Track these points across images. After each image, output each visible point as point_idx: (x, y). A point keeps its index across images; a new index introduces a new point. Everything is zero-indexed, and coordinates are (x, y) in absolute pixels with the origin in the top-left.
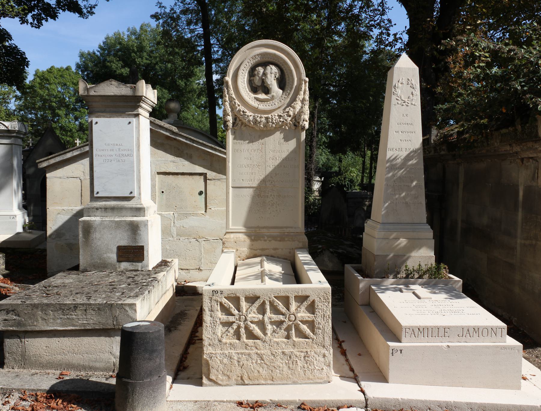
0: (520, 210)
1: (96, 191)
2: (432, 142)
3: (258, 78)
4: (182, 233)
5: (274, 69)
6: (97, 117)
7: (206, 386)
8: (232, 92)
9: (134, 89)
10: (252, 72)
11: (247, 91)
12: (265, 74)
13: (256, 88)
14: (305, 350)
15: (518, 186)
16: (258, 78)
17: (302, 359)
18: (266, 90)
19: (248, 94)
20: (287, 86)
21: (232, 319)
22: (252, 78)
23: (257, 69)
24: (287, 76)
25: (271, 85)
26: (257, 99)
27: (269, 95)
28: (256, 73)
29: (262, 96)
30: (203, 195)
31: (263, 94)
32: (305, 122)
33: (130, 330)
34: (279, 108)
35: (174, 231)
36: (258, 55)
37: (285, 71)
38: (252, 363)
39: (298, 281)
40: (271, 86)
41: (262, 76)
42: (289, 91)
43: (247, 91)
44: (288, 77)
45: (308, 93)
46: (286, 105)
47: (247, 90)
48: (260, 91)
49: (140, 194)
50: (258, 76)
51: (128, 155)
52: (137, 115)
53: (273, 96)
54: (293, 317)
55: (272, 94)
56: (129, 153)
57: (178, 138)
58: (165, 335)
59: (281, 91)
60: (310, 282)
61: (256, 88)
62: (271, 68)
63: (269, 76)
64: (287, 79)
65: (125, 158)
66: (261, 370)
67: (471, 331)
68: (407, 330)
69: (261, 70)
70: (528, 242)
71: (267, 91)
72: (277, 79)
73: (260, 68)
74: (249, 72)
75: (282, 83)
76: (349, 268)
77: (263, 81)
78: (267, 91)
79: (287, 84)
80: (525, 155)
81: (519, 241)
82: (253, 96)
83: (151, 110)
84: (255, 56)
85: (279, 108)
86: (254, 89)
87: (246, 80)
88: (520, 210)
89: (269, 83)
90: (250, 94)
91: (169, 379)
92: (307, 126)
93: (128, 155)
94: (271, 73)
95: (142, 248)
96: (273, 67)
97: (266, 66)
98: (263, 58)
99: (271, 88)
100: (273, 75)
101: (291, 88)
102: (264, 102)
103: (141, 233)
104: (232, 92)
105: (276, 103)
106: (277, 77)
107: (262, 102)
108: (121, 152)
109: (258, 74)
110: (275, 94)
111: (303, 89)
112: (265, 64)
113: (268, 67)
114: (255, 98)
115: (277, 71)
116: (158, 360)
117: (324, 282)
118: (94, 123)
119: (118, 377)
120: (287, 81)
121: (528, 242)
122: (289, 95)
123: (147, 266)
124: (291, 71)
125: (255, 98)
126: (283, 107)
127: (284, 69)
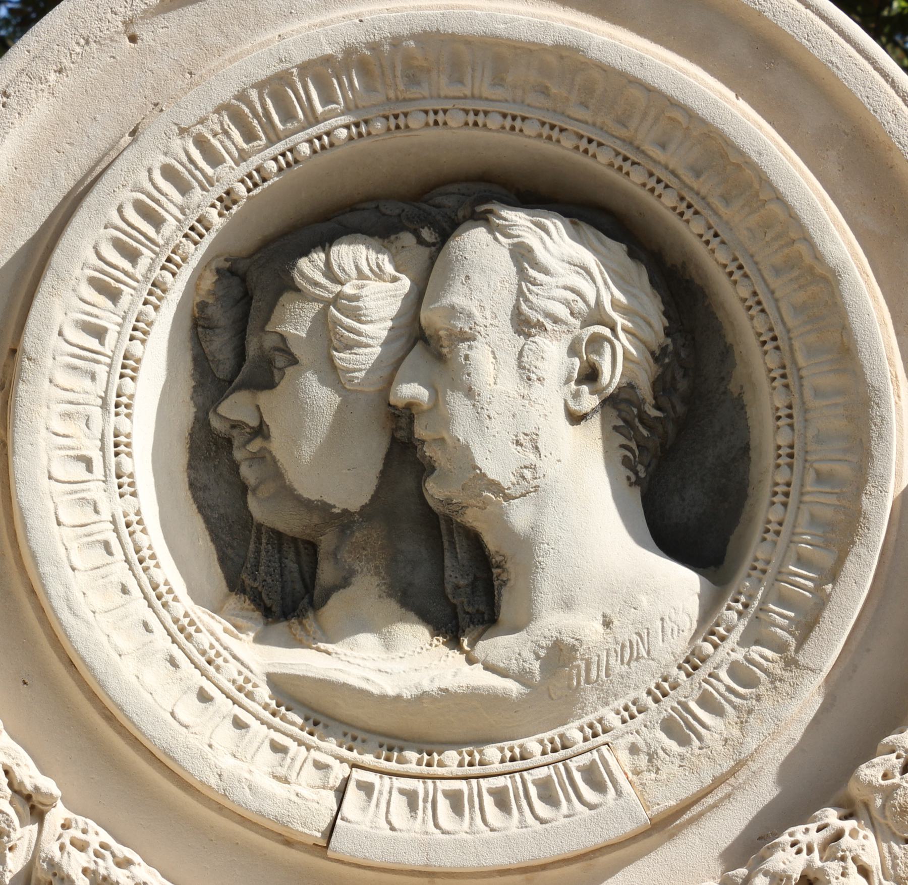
3: (321, 398)
5: (568, 261)
8: (295, 730)
10: (238, 325)
11: (157, 596)
12: (423, 340)
13: (308, 550)
16: (321, 398)
18: (455, 575)
19: (184, 630)
20: (765, 510)
22: (236, 407)
23: (310, 267)
24: (756, 363)
25: (531, 487)
26: (316, 709)
27: (498, 646)
28: (296, 323)
29: (392, 659)
31: (414, 637)
34: (664, 826)
36: (320, 70)
37: (731, 295)
40: (520, 515)
41: (391, 369)
42: (802, 581)
43: (157, 596)
44: (785, 375)
46: (762, 791)
47: (168, 571)
48: (366, 588)
50: (333, 375)
53: (559, 654)
55: (551, 622)
57: (751, 667)
58: (515, 629)
59: (682, 583)
61: (308, 550)
62: (522, 255)
63: (489, 360)
64: (765, 403)
69: (367, 283)
71: (462, 579)
72: (617, 404)
73: (351, 255)
74: (197, 325)
77: (405, 447)
78: (462, 579)
79: (768, 473)
82: (260, 657)
84: (277, 86)
85: (664, 826)
86: (275, 573)
87: (142, 427)
89: (495, 460)
90: (213, 627)
94: (523, 325)
96: (557, 244)
97: (447, 230)
98: (397, 121)
99: (526, 545)
100: (553, 356)
101: (843, 532)
102: (429, 745)
104: (295, 730)
105: (619, 762)
106: (611, 376)
107: (391, 742)
109: (329, 337)
110: (585, 627)
112: (423, 210)
113: (475, 243)
114: (288, 693)
115: (610, 295)
120: (768, 436)
122: (807, 625)
124: (824, 281)
125: (288, 693)
126: (730, 822)
127: (712, 262)
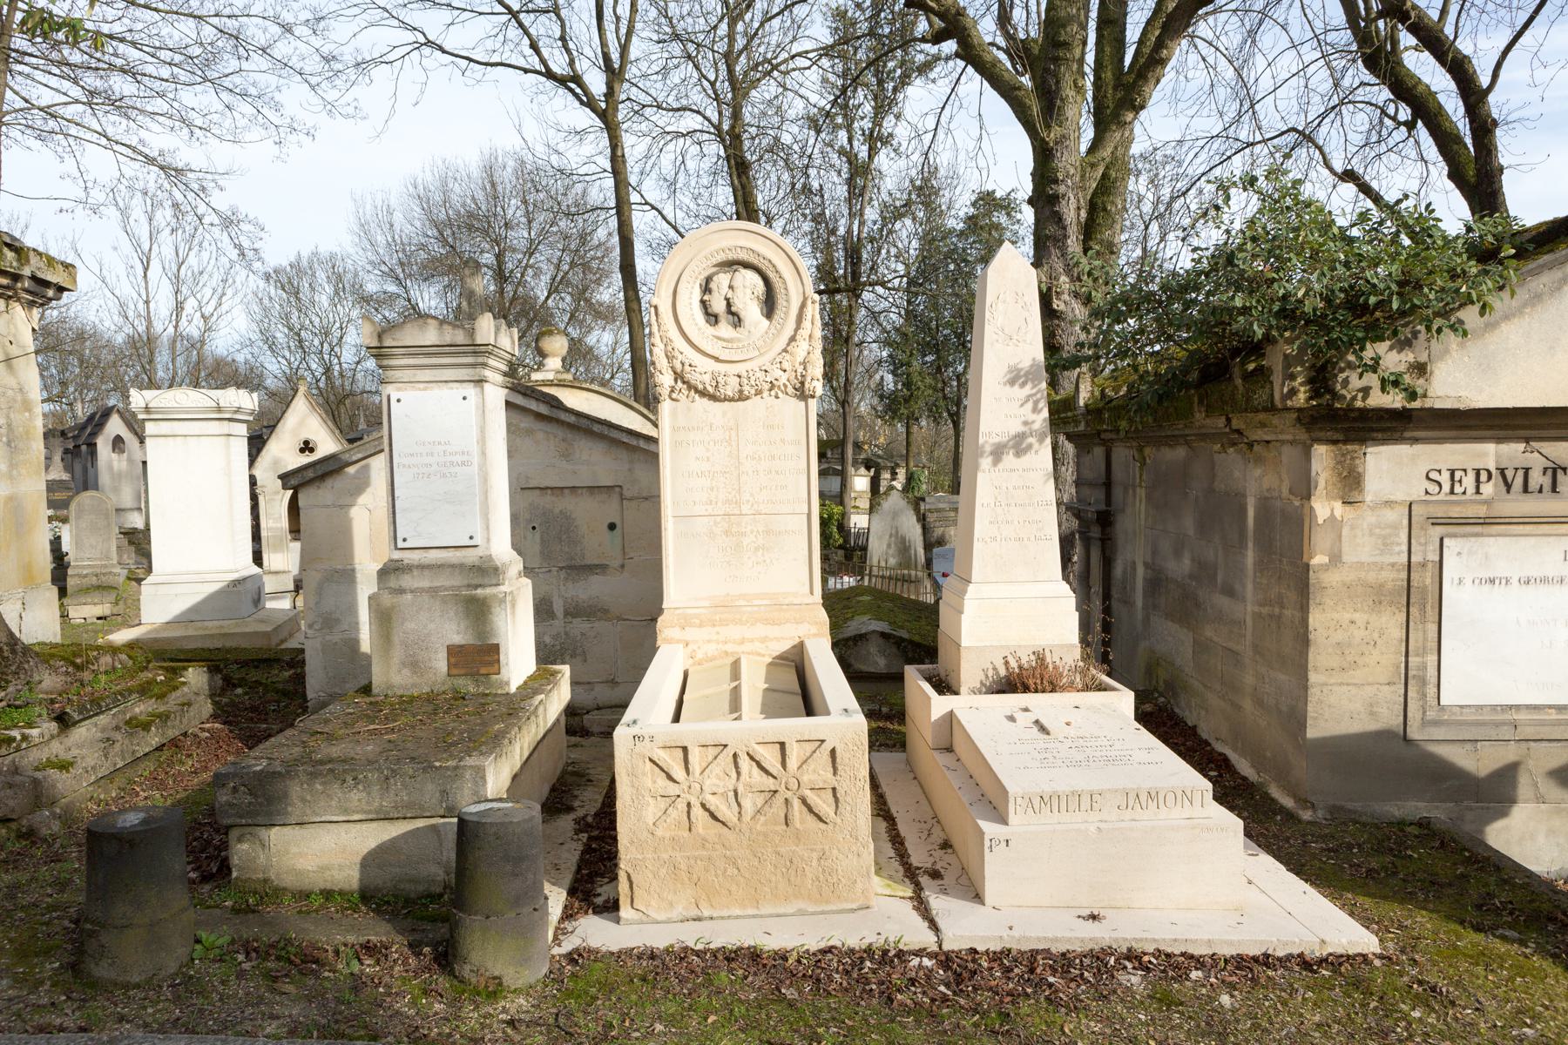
0: (1250, 545)
1: (400, 537)
2: (1082, 403)
4: (573, 612)
6: (399, 389)
7: (630, 923)
9: (471, 333)
14: (819, 847)
15: (1244, 496)
17: (815, 863)
21: (673, 789)
30: (618, 530)
32: (815, 383)
33: (475, 819)
35: (558, 608)
38: (716, 876)
39: (809, 711)
45: (818, 323)
49: (488, 540)
51: (463, 463)
52: (480, 382)
54: (793, 785)
56: (465, 458)
60: (828, 713)
65: (457, 469)
66: (734, 888)
67: (1143, 797)
68: (1019, 800)
69: (722, 280)
70: (1265, 610)
75: (769, 304)
76: (911, 672)
78: (736, 319)
80: (1260, 435)
81: (1249, 608)
83: (504, 368)
86: (712, 318)
88: (1250, 545)
91: (556, 899)
92: (819, 391)
93: (463, 463)
95: (495, 649)
100: (749, 292)
103: (495, 619)
108: (449, 458)
111: (809, 317)
112: (731, 265)
116: (530, 876)
117: (855, 712)
118: (393, 401)
119: (252, 391)
121: (1265, 610)
123: (507, 683)
